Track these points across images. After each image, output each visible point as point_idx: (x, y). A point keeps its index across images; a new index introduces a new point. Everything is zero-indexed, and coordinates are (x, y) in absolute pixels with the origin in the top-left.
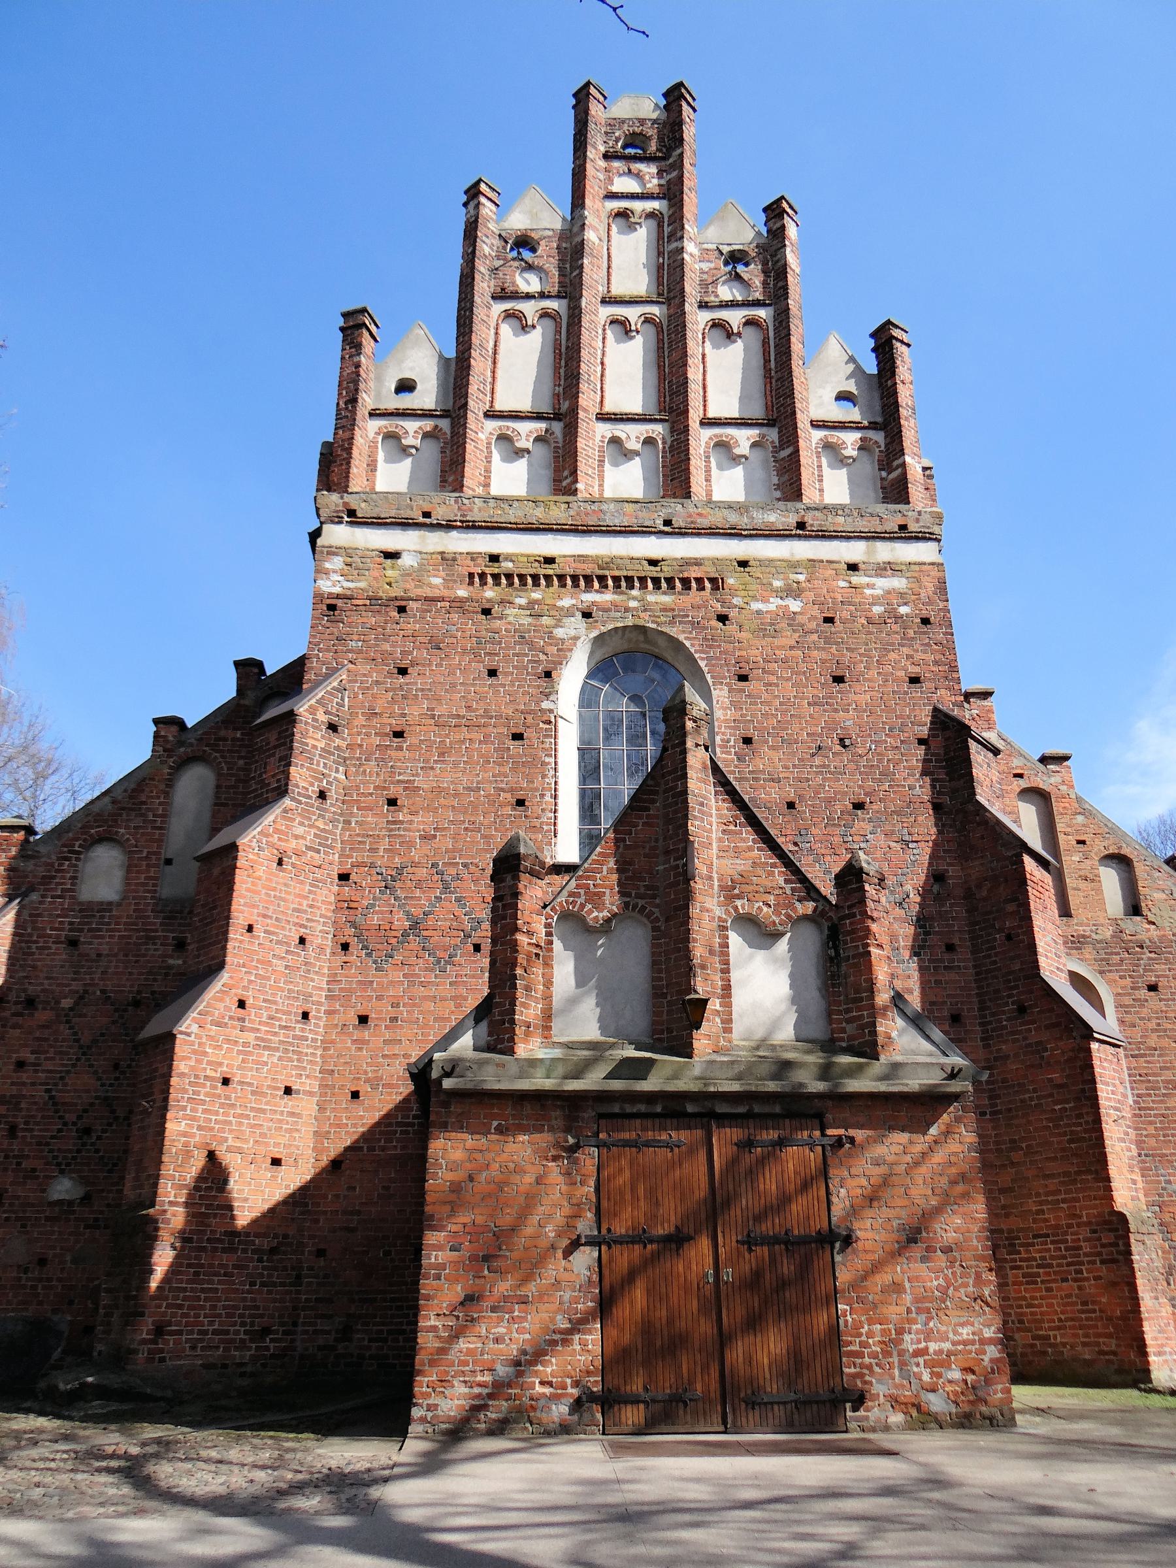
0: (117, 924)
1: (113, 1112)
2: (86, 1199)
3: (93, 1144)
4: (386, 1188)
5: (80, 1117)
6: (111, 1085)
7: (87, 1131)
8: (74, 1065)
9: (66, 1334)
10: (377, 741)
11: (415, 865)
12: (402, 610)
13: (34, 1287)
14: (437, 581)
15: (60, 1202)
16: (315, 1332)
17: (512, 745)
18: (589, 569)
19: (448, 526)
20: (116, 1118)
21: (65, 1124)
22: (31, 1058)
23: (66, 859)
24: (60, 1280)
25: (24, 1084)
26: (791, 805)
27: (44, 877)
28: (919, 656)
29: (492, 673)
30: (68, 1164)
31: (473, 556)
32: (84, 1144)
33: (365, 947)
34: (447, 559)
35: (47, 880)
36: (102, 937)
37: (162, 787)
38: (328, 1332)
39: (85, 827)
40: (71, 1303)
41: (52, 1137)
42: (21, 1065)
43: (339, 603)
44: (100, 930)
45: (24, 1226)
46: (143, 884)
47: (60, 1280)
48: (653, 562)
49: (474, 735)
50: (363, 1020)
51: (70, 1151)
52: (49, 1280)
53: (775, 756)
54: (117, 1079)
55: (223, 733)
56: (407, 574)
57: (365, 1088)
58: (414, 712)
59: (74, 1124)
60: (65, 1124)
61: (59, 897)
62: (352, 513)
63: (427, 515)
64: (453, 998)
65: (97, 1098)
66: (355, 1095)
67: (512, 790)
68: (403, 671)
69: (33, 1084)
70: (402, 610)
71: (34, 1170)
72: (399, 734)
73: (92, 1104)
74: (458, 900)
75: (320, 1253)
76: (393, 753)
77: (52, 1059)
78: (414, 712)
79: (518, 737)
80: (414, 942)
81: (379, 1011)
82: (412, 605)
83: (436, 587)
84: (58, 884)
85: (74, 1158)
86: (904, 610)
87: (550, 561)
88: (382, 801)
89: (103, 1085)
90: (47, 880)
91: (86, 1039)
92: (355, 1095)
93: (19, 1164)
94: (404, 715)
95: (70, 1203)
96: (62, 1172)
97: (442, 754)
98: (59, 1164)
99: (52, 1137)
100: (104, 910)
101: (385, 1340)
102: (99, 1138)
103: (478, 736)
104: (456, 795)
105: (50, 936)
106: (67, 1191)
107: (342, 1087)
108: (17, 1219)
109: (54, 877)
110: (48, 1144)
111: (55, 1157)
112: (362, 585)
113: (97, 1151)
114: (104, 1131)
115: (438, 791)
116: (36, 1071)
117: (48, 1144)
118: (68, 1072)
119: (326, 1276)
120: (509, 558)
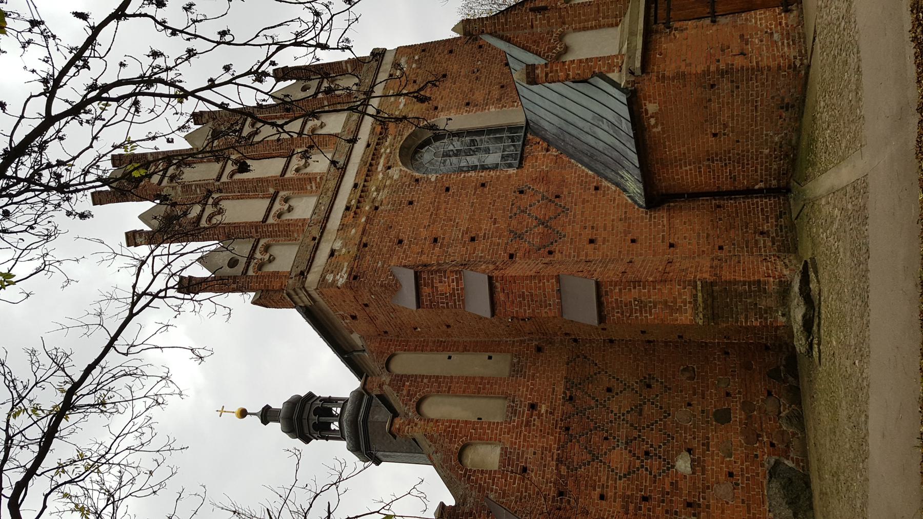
0: (515, 443)
1: (635, 439)
2: (689, 451)
3: (655, 450)
4: (685, 223)
5: (638, 458)
6: (618, 441)
7: (647, 453)
8: (605, 463)
9: (777, 458)
10: (437, 249)
11: (509, 225)
12: (365, 245)
13: (748, 479)
14: (354, 231)
15: (693, 467)
16: (765, 247)
17: (451, 192)
18: (365, 170)
19: (323, 229)
20: (639, 436)
21: (642, 466)
22: (598, 490)
23: (469, 478)
24: (742, 464)
25: (615, 493)
26: (502, 87)
27: (479, 492)
28: (440, 51)
29: (411, 203)
30: (668, 463)
31: (344, 216)
32: (656, 455)
33: (552, 243)
34: (343, 227)
35: (481, 489)
36: (523, 452)
37: (431, 424)
38: (764, 241)
39: (451, 469)
40: (756, 456)
41: (651, 474)
42: (602, 497)
43: (354, 274)
44: (518, 454)
45: (708, 487)
46: (492, 431)
47: (742, 464)
48: (368, 145)
49: (443, 207)
50: (592, 241)
51: (660, 463)
52: (742, 470)
53: (477, 93)
54: (614, 438)
55: (405, 392)
56: (345, 245)
57: (629, 237)
58: (424, 233)
59: (642, 461)
60: (642, 466)
61: (494, 480)
62: (302, 273)
63: (314, 239)
64: (583, 203)
65: (626, 449)
66: (633, 241)
67: (476, 189)
68: (400, 242)
69: (616, 488)
70: (365, 245)
71: (672, 484)
72: (435, 240)
73: (630, 452)
74: (530, 206)
75: (721, 248)
76: (445, 241)
77: (600, 478)
78: (424, 233)
79: (448, 189)
80: (552, 223)
81: (588, 234)
82: (364, 240)
83: (356, 233)
84: (485, 482)
85: (664, 460)
86: (416, 58)
87: (356, 186)
88: (472, 243)
89: (618, 446)
90: (481, 489)
91: (589, 457)
92: (633, 241)
93: (668, 493)
94: (425, 238)
95: (693, 461)
96: (673, 467)
97: (451, 220)
98: (668, 469)
99: (651, 474)
100: (506, 452)
101: (767, 217)
102: (652, 446)
103: (443, 206)
104: (474, 211)
105: (519, 484)
106: (686, 462)
107: (629, 247)
108: (704, 492)
109: (480, 485)
110: (655, 476)
111: (664, 471)
112: (346, 264)
113: (660, 447)
114: (647, 444)
115: (471, 219)
116: (607, 486)
117: (655, 476)
118: (609, 467)
119: (734, 244)
120: (349, 201)
